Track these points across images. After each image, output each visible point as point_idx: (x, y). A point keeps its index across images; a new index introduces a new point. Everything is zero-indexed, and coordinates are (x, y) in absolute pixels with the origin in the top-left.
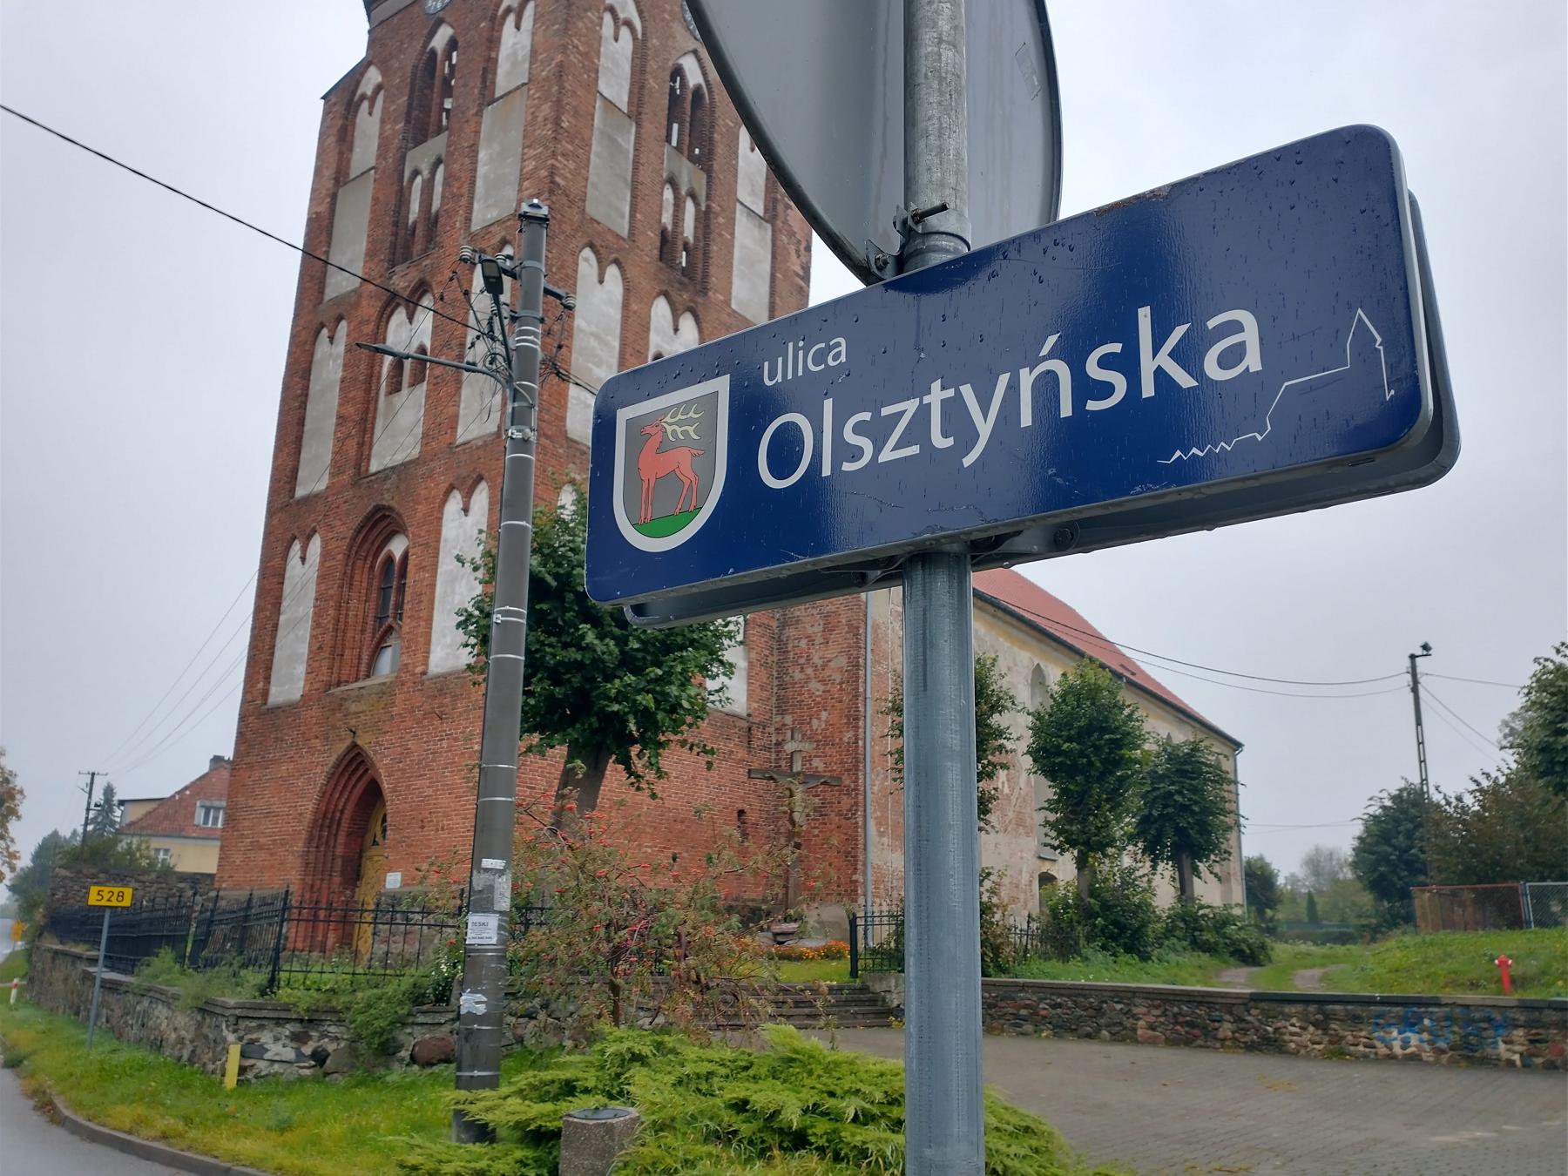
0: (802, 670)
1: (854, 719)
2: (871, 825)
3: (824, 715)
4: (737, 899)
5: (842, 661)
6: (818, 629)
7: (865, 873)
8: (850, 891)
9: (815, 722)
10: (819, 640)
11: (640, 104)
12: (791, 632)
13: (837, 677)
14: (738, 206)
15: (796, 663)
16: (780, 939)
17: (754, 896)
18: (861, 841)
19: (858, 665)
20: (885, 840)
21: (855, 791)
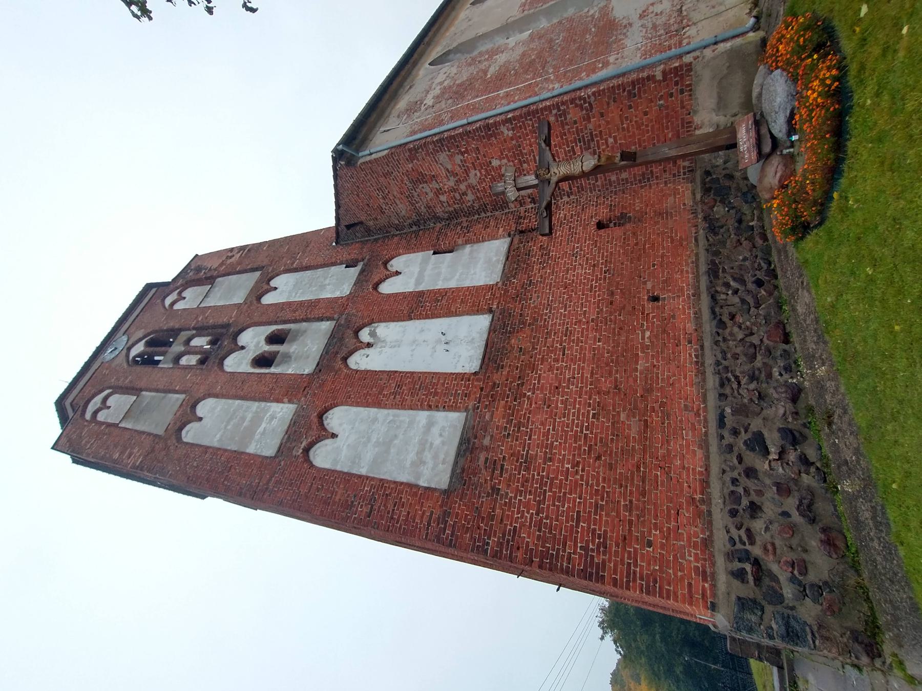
0: (465, 194)
1: (489, 130)
2: (594, 78)
3: (495, 163)
4: (695, 213)
5: (443, 157)
6: (426, 188)
7: (652, 66)
8: (725, 637)
10: (434, 185)
11: (133, 388)
12: (439, 210)
13: (458, 158)
14: (202, 305)
15: (461, 202)
16: (767, 148)
17: (688, 194)
18: (615, 82)
19: (440, 140)
20: (611, 59)
21: (560, 105)
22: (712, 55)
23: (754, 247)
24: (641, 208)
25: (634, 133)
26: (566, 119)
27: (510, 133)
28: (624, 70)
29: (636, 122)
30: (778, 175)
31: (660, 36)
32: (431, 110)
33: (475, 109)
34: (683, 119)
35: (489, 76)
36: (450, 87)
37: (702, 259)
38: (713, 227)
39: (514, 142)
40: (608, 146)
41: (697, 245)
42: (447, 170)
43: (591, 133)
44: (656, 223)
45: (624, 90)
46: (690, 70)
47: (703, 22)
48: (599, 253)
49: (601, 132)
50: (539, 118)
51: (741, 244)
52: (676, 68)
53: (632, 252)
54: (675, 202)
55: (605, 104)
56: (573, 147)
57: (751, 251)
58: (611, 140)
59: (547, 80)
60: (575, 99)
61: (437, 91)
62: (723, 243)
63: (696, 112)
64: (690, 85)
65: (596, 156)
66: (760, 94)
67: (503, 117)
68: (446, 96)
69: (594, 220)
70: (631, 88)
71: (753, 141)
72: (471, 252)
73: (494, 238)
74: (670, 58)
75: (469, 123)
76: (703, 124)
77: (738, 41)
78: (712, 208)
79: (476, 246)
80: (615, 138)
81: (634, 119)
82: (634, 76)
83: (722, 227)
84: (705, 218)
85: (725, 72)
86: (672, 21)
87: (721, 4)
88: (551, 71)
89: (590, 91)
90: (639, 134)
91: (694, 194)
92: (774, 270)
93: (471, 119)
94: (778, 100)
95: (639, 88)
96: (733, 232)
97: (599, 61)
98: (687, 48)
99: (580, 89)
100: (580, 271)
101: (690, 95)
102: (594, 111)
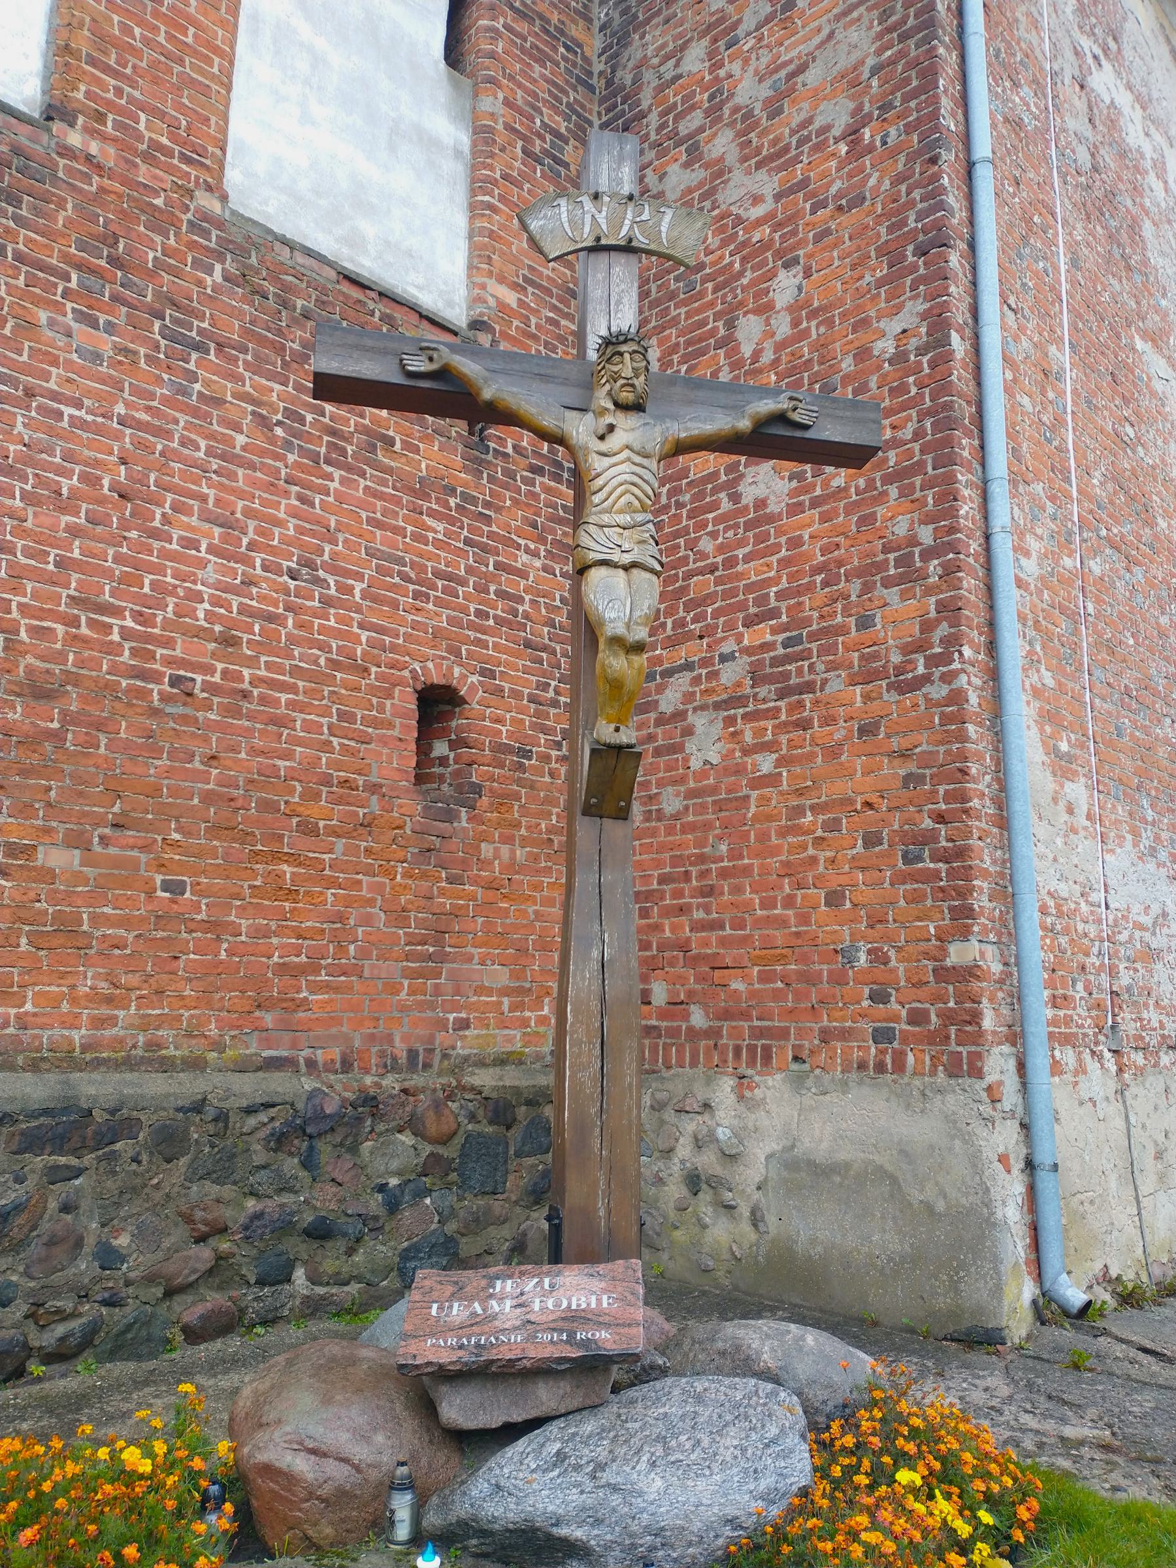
0: (694, 155)
1: (923, 248)
2: (1021, 711)
3: (785, 287)
7: (1008, 933)
9: (749, 329)
13: (836, 114)
16: (460, 1409)
17: (513, 1040)
18: (982, 783)
20: (1077, 791)
22: (990, 1154)
23: (169, 1294)
24: (485, 864)
25: (775, 851)
26: (887, 583)
27: (886, 347)
28: (1018, 823)
29: (814, 860)
30: (301, 1465)
31: (1113, 973)
32: (1069, 72)
33: (1026, 228)
34: (784, 1034)
35: (1139, 344)
36: (1137, 190)
37: (155, 1085)
38: (305, 1132)
39: (847, 365)
40: (746, 752)
41: (242, 1067)
42: (802, 69)
43: (809, 687)
44: (399, 916)
45: (940, 818)
46: (954, 1071)
47: (1120, 1123)
48: (295, 671)
49: (805, 725)
50: (920, 467)
51: (201, 1239)
52: (975, 1017)
53: (267, 806)
54: (481, 990)
55: (906, 743)
56: (774, 614)
57: (150, 1279)
58: (766, 763)
59: (1063, 541)
60: (954, 623)
61: (1134, 134)
62: (221, 1169)
63: (798, 1082)
64: (899, 1066)
65: (641, 634)
66: (743, 1365)
67: (959, 314)
68: (1107, 156)
69: (468, 682)
70: (942, 847)
71: (513, 1345)
72: (431, 143)
73: (483, 254)
74: (1017, 998)
75: (970, 168)
76: (753, 1105)
77: (1016, 1247)
78: (413, 1125)
79: (455, 171)
80: (772, 780)
81: (823, 856)
82: (986, 859)
83: (308, 1163)
84: (370, 1103)
85: (915, 1195)
86: (1153, 1016)
87: (1162, 1177)
88: (1096, 567)
89: (972, 684)
90: (765, 871)
91: (501, 1061)
92: (19, 1373)
93: (985, 179)
94: (654, 1484)
95: (936, 875)
96: (270, 1205)
97: (1082, 746)
98: (1039, 1062)
99: (992, 647)
100: (210, 574)
101: (862, 1066)
102: (894, 697)
